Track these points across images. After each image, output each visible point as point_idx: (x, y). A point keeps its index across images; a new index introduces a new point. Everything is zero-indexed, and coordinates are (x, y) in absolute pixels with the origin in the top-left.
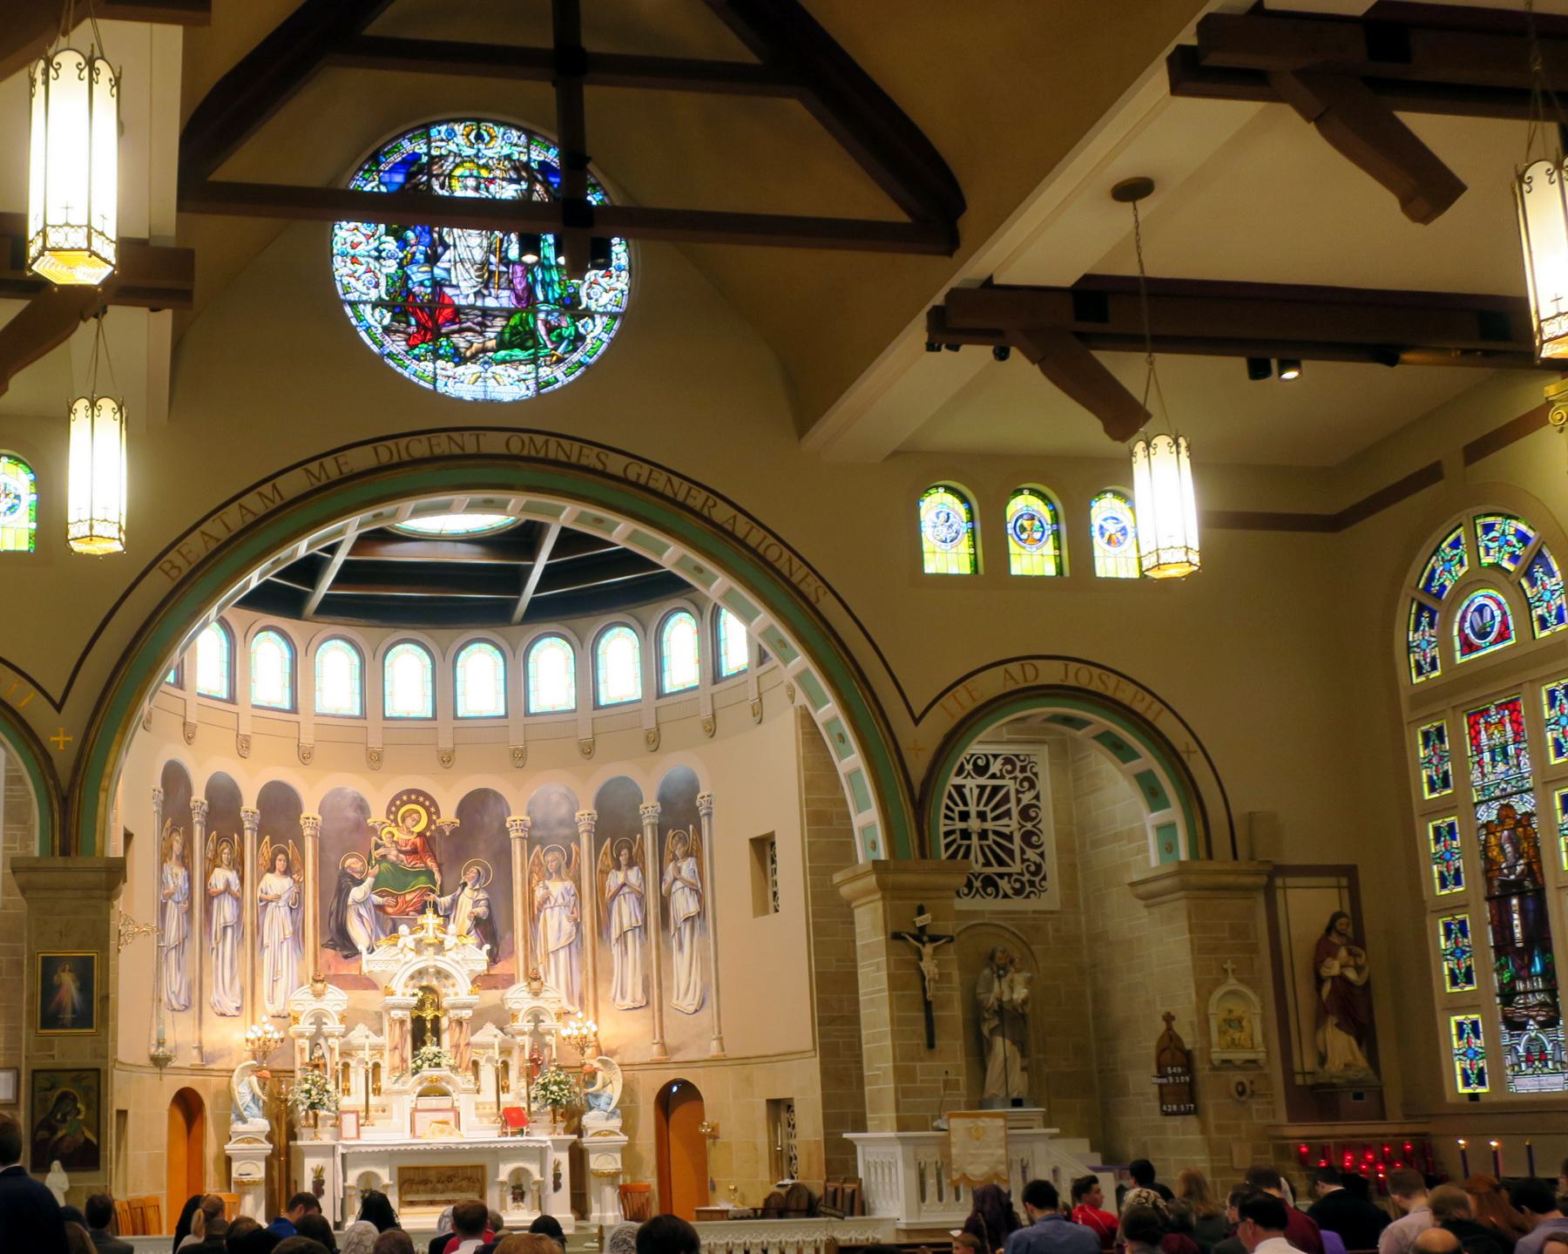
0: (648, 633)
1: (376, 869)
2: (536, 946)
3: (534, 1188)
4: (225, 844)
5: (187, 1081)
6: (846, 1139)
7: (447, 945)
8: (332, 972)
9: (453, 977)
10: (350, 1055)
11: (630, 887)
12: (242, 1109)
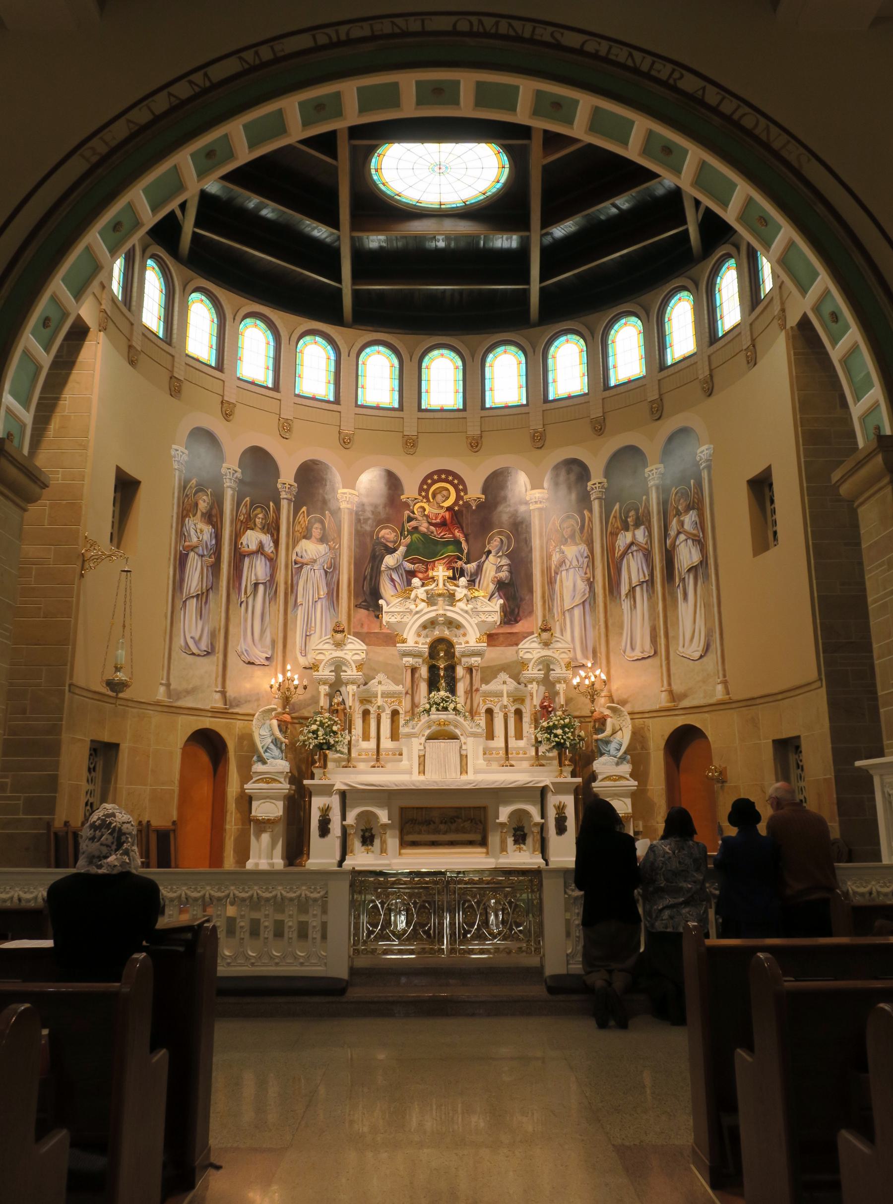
0: (651, 314)
1: (408, 540)
2: (553, 606)
3: (536, 830)
4: (259, 510)
5: (207, 723)
6: (859, 768)
7: (458, 596)
8: (365, 630)
9: (464, 627)
10: (370, 702)
11: (637, 545)
12: (262, 751)
